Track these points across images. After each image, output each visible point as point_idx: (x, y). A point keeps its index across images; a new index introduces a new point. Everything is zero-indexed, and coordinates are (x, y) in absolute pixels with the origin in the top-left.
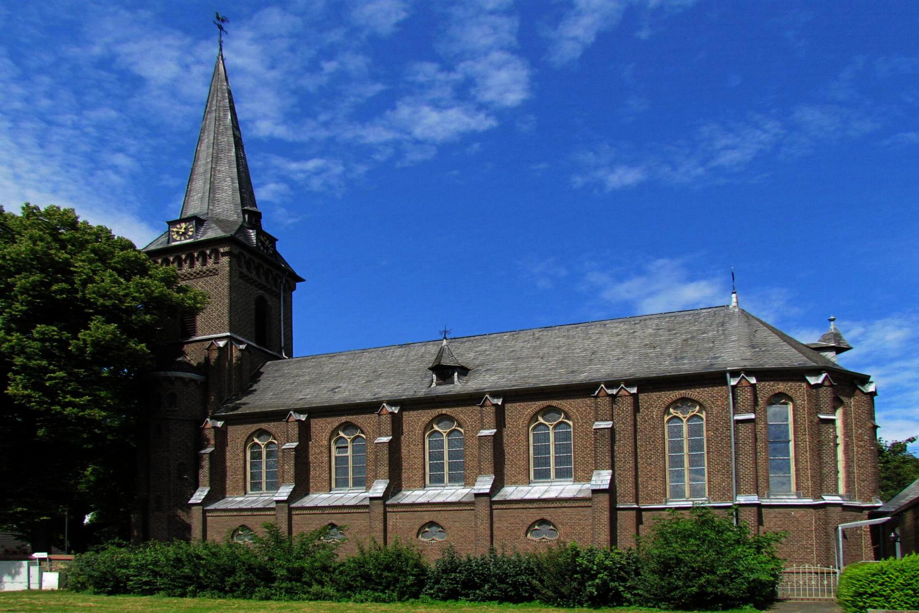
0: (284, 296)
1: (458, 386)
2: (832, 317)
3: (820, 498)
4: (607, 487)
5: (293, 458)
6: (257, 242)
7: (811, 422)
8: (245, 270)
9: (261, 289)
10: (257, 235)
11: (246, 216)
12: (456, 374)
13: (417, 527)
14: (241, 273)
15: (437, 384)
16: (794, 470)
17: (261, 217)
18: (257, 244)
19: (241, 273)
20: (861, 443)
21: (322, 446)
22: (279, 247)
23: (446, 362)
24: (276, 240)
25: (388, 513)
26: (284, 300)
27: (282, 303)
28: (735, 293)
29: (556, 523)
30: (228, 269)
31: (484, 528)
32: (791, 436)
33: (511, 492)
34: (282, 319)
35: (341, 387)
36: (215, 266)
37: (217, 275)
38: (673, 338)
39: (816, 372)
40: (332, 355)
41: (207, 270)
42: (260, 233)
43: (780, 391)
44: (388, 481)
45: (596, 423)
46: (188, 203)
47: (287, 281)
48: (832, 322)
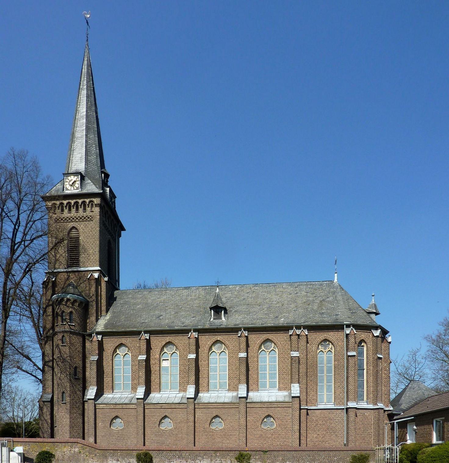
1: (224, 321)
2: (373, 294)
3: (376, 404)
5: (144, 367)
7: (373, 358)
11: (103, 175)
13: (210, 419)
15: (214, 319)
16: (366, 387)
21: (156, 359)
25: (97, 410)
27: (117, 244)
28: (336, 273)
29: (275, 417)
30: (98, 217)
31: (243, 421)
32: (365, 367)
33: (254, 396)
36: (91, 214)
37: (92, 221)
41: (86, 216)
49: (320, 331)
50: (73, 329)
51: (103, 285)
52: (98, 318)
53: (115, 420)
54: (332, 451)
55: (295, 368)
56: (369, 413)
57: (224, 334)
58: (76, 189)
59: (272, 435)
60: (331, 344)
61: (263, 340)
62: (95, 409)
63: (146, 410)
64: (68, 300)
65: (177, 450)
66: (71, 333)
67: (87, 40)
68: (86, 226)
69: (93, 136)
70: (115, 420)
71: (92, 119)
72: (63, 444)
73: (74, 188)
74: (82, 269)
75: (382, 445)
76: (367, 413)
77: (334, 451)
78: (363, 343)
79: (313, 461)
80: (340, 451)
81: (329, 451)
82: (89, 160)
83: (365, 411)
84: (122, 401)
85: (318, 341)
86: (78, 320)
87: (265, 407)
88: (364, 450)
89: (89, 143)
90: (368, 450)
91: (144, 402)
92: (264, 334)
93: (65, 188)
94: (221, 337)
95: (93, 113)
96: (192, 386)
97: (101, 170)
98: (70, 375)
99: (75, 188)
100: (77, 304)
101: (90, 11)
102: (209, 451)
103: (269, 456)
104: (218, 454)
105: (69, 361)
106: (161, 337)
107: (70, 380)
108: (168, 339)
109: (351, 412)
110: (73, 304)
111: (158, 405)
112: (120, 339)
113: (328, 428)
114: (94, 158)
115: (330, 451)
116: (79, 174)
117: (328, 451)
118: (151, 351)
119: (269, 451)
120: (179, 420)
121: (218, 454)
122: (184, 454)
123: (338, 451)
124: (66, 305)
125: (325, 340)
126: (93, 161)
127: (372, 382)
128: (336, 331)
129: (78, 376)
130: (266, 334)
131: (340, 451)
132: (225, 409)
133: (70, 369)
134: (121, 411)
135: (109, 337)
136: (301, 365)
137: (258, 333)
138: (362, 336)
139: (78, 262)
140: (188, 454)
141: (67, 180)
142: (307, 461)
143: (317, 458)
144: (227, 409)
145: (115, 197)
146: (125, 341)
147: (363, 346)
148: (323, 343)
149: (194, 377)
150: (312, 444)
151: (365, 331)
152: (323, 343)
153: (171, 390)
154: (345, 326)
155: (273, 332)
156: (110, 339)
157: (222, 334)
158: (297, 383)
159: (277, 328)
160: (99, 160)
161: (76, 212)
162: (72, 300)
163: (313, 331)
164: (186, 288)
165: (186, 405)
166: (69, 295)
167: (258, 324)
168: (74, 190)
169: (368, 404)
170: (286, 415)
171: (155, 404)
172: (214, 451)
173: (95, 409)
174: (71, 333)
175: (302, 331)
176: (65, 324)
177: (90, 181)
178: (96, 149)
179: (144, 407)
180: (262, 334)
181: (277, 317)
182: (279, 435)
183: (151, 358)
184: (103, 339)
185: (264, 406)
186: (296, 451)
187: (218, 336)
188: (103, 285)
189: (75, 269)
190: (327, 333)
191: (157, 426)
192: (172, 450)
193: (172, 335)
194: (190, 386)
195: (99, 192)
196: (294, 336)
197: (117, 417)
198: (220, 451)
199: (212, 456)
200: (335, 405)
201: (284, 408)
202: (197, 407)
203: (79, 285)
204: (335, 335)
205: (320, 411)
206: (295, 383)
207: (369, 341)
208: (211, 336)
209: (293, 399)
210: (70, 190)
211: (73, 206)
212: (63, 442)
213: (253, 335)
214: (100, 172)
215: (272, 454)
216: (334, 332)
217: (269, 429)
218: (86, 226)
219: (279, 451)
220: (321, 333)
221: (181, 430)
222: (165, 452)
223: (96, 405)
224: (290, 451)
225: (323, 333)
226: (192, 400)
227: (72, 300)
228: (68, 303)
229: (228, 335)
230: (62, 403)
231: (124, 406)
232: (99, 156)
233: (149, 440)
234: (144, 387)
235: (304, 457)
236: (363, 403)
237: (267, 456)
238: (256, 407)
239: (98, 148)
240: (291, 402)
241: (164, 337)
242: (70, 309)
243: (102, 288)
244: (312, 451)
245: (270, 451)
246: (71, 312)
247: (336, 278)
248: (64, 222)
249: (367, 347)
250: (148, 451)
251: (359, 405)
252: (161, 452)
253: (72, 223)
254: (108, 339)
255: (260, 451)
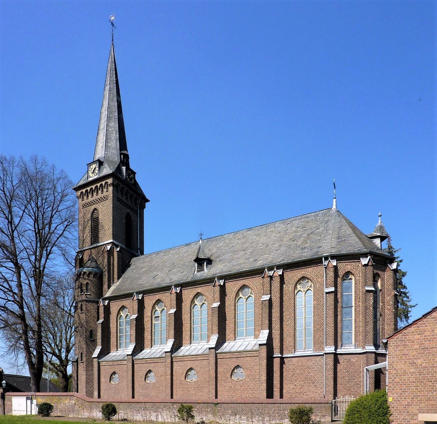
0: (139, 213)
1: (207, 272)
2: (380, 214)
3: (364, 348)
4: (265, 342)
6: (126, 175)
8: (120, 196)
9: (128, 208)
10: (126, 170)
11: (122, 156)
12: (205, 263)
13: (185, 372)
14: (118, 198)
15: (198, 271)
17: (128, 158)
18: (126, 177)
19: (118, 198)
20: (389, 307)
22: (138, 178)
23: (201, 256)
24: (136, 173)
25: (101, 367)
26: (139, 216)
28: (335, 198)
34: (139, 229)
35: (158, 275)
38: (303, 234)
39: (365, 255)
40: (157, 253)
42: (128, 169)
43: (348, 270)
44: (173, 340)
45: (263, 296)
46: (96, 150)
47: (141, 201)
48: (380, 217)
49: (297, 269)
50: (89, 298)
51: (116, 255)
52: (111, 285)
53: (114, 375)
54: (282, 403)
55: (265, 312)
56: (356, 358)
57: (203, 285)
58: (96, 175)
59: (242, 386)
60: (310, 281)
61: (239, 287)
62: (216, 359)
63: (135, 365)
64: (85, 273)
65: (142, 403)
66: (87, 301)
67: (113, 39)
68: (103, 206)
69: (114, 124)
70: (114, 375)
71: (114, 109)
72: (65, 397)
73: (94, 175)
74: (102, 243)
75: (342, 397)
76: (354, 359)
77: (285, 403)
78: (350, 276)
79: (262, 415)
80: (290, 403)
81: (279, 403)
82: (109, 146)
83: (351, 356)
84: (119, 358)
85: (295, 280)
86: (93, 289)
87: (234, 357)
88: (318, 403)
89: (110, 131)
90: (323, 403)
91: (132, 358)
92: (240, 280)
93: (88, 177)
94: (201, 289)
95: (114, 104)
96: (172, 339)
97: (120, 152)
98: (86, 337)
99: (95, 174)
100: (92, 276)
101: (114, 14)
102: (167, 403)
103: (219, 409)
104: (175, 406)
105: (85, 326)
106: (152, 296)
107: (86, 342)
108: (157, 296)
109: (329, 358)
110: (88, 276)
111: (144, 360)
112: (122, 301)
113: (306, 378)
114: (115, 143)
115: (280, 403)
116: (98, 161)
117: (277, 403)
118: (145, 310)
119: (219, 403)
120: (160, 374)
121: (175, 406)
122: (148, 405)
123: (289, 403)
124: (83, 278)
125: (303, 278)
126: (113, 146)
127: (361, 321)
128: (315, 266)
129: (94, 339)
130: (242, 280)
131: (290, 403)
132: (198, 361)
133: (86, 332)
134: (117, 368)
135: (114, 301)
136: (275, 308)
137: (235, 280)
138: (347, 267)
139: (98, 239)
140: (150, 406)
141: (90, 169)
142: (257, 415)
143: (267, 411)
144: (199, 361)
145: (134, 173)
146: (126, 303)
147: (351, 279)
148: (301, 282)
149: (173, 331)
150: (289, 396)
151: (351, 261)
152: (301, 282)
153: (161, 345)
154: (323, 258)
155: (249, 277)
156: (115, 303)
157: (201, 286)
158: (266, 329)
159: (253, 272)
160: (119, 144)
161: (96, 195)
162: (87, 272)
163: (289, 270)
164: (187, 245)
165: (126, 361)
166: (85, 268)
167: (235, 269)
168: (95, 176)
169: (355, 348)
170: (254, 365)
171: (141, 359)
172: (171, 403)
173: (216, 359)
174: (87, 301)
175: (275, 272)
176: (83, 294)
177: (106, 165)
178: (116, 135)
179: (216, 356)
180: (239, 281)
181: (256, 260)
182: (248, 386)
183: (145, 316)
184: (110, 304)
185: (233, 357)
186: (245, 403)
187: (198, 288)
188: (116, 255)
189: (95, 245)
190: (304, 269)
191: (144, 380)
192: (139, 402)
193: (161, 293)
194: (170, 340)
195: (110, 173)
196: (265, 279)
197: (238, 367)
198: (177, 403)
199: (170, 408)
200: (314, 351)
201: (253, 357)
202: (174, 361)
203: (98, 259)
204: (314, 271)
205: (298, 358)
206: (265, 329)
207: (357, 272)
208: (193, 289)
209: (260, 347)
210: (93, 177)
211: (95, 190)
212: (65, 396)
213: (231, 282)
214: (119, 154)
215: (222, 406)
216: (313, 268)
217: (239, 380)
218: (103, 206)
219: (229, 403)
220: (298, 270)
221: (162, 383)
222: (133, 404)
223: (100, 363)
224: (239, 403)
225: (300, 270)
226: (169, 354)
227: (87, 272)
228: (85, 276)
229: (207, 287)
230: (81, 362)
231: (119, 363)
232: (118, 140)
233: (137, 393)
234: (134, 344)
235: (253, 410)
236: (349, 347)
237: (217, 408)
238: (226, 357)
239: (118, 133)
240: (258, 351)
241: (154, 296)
242: (87, 281)
243: (115, 258)
244: (261, 403)
245: (220, 403)
246: (87, 284)
247: (334, 203)
248: (89, 206)
249: (355, 279)
250: (113, 403)
251: (343, 350)
252: (130, 404)
253: (94, 206)
254: (114, 303)
255: (211, 403)
